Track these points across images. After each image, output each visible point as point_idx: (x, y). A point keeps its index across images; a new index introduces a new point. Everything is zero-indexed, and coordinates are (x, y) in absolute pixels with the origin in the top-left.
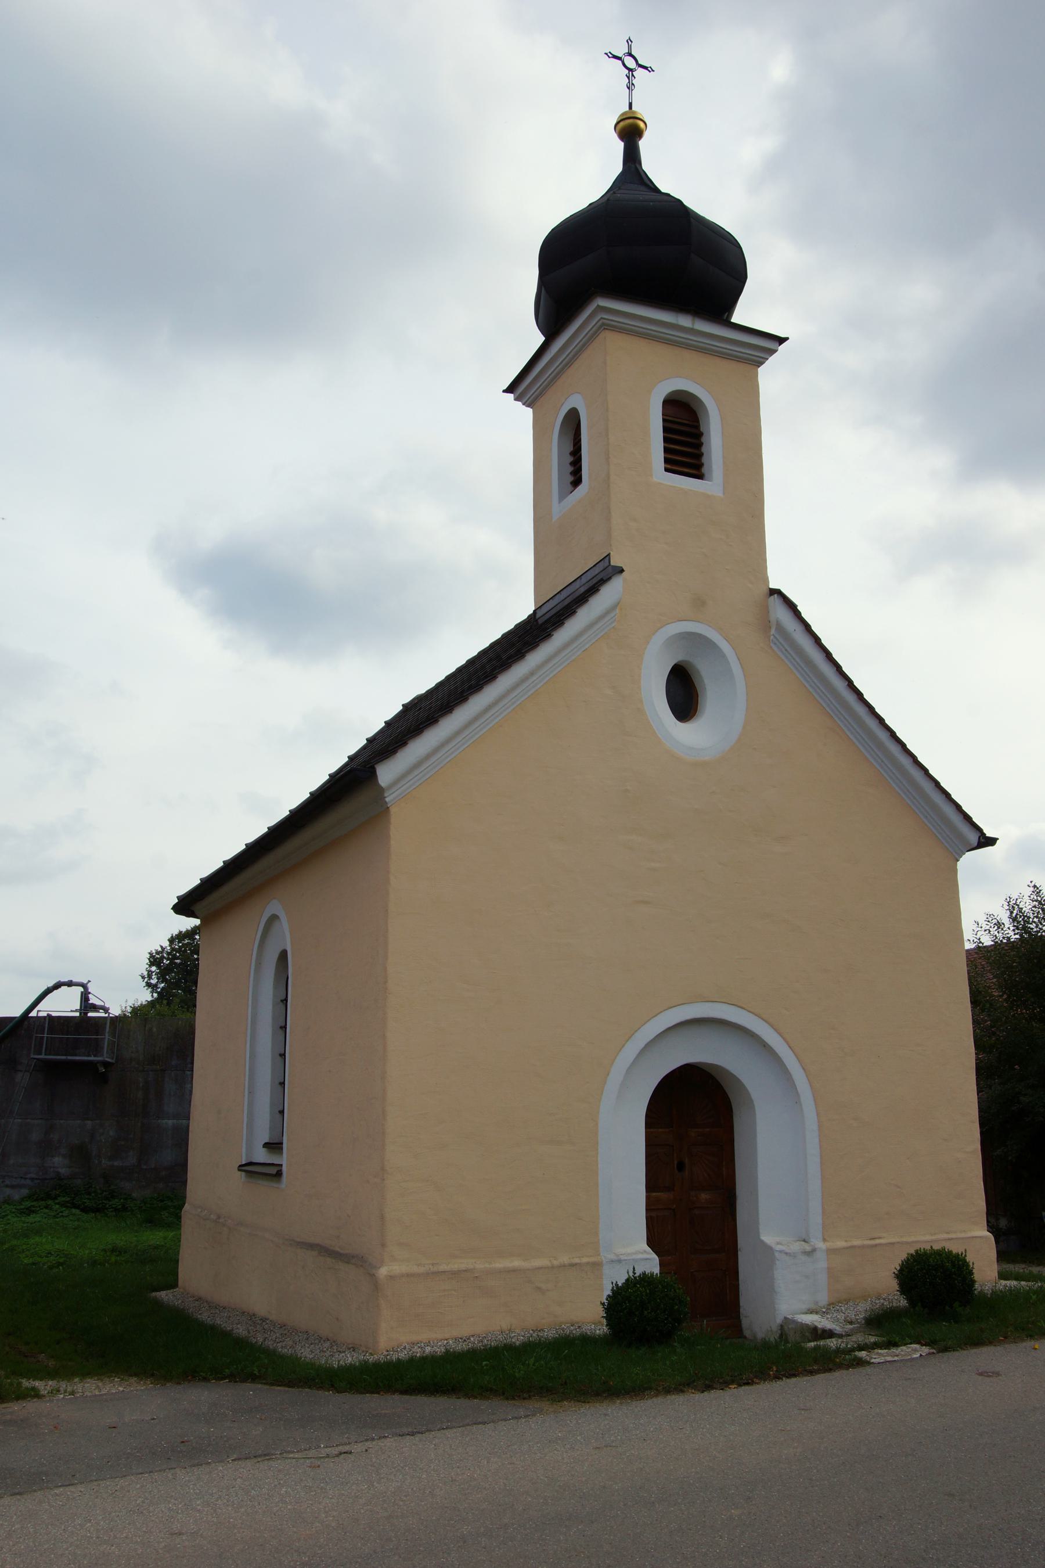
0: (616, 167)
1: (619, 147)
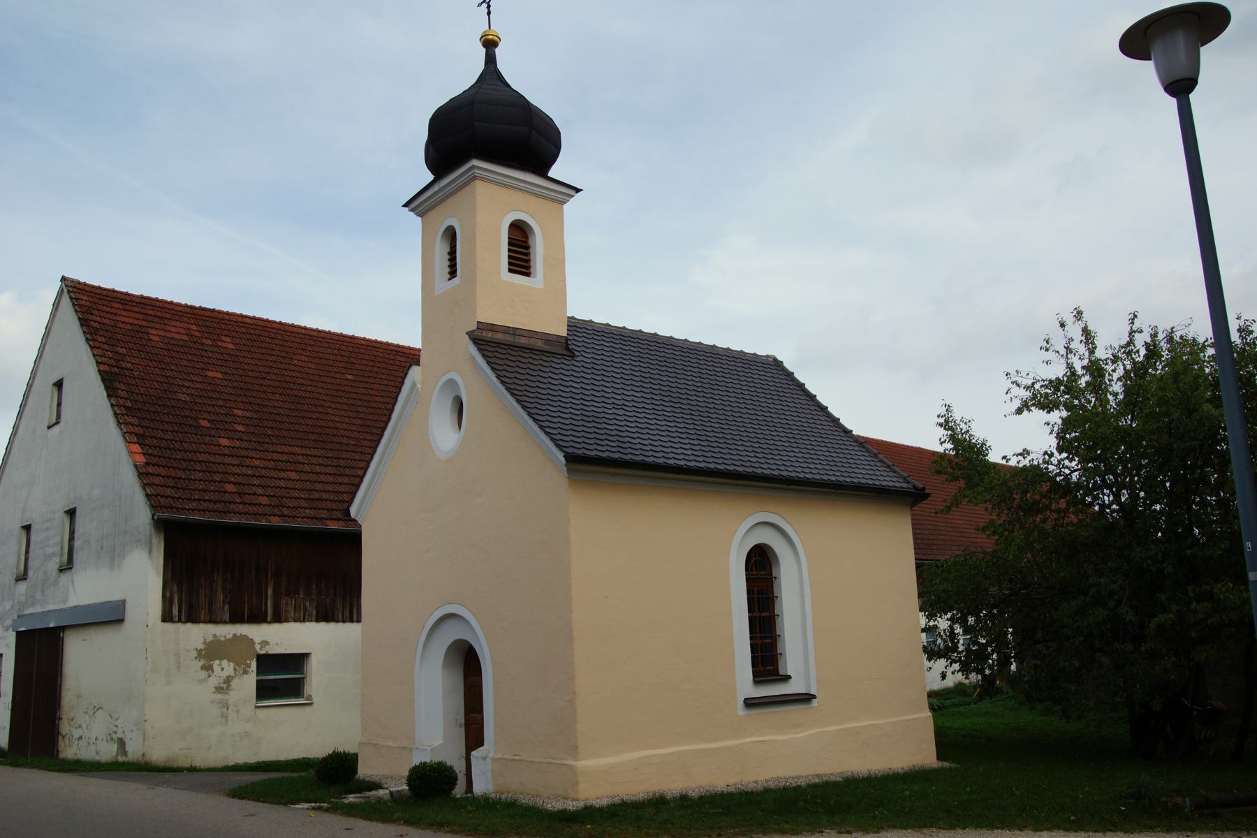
1: (482, 51)
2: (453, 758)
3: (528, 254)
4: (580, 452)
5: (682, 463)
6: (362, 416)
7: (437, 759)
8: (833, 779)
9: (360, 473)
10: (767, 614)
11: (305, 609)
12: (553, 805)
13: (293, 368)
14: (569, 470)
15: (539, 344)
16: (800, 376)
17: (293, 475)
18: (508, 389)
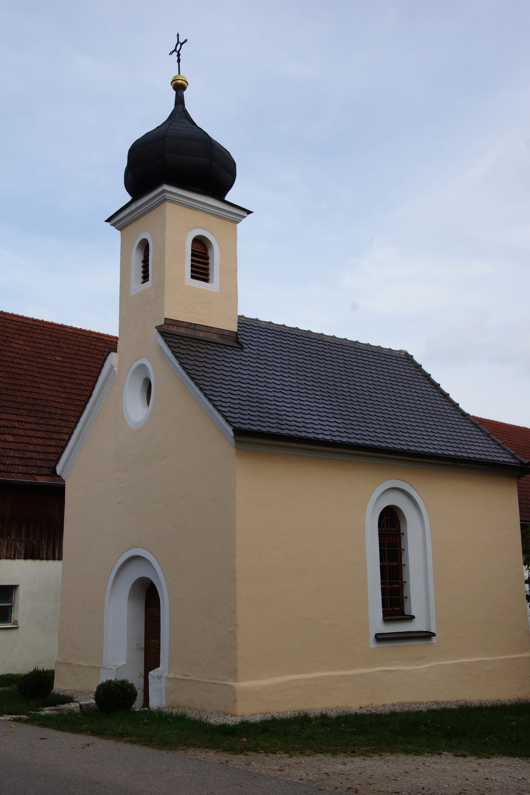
0: (171, 106)
2: (134, 678)
3: (207, 264)
4: (246, 427)
5: (328, 438)
6: (68, 390)
7: (120, 678)
8: (449, 706)
9: (66, 437)
10: (395, 564)
11: (16, 548)
12: (215, 720)
13: (12, 350)
14: (236, 441)
15: (215, 338)
16: (427, 368)
17: (10, 438)
18: (188, 374)
